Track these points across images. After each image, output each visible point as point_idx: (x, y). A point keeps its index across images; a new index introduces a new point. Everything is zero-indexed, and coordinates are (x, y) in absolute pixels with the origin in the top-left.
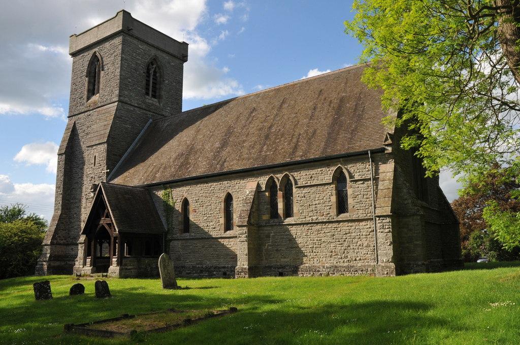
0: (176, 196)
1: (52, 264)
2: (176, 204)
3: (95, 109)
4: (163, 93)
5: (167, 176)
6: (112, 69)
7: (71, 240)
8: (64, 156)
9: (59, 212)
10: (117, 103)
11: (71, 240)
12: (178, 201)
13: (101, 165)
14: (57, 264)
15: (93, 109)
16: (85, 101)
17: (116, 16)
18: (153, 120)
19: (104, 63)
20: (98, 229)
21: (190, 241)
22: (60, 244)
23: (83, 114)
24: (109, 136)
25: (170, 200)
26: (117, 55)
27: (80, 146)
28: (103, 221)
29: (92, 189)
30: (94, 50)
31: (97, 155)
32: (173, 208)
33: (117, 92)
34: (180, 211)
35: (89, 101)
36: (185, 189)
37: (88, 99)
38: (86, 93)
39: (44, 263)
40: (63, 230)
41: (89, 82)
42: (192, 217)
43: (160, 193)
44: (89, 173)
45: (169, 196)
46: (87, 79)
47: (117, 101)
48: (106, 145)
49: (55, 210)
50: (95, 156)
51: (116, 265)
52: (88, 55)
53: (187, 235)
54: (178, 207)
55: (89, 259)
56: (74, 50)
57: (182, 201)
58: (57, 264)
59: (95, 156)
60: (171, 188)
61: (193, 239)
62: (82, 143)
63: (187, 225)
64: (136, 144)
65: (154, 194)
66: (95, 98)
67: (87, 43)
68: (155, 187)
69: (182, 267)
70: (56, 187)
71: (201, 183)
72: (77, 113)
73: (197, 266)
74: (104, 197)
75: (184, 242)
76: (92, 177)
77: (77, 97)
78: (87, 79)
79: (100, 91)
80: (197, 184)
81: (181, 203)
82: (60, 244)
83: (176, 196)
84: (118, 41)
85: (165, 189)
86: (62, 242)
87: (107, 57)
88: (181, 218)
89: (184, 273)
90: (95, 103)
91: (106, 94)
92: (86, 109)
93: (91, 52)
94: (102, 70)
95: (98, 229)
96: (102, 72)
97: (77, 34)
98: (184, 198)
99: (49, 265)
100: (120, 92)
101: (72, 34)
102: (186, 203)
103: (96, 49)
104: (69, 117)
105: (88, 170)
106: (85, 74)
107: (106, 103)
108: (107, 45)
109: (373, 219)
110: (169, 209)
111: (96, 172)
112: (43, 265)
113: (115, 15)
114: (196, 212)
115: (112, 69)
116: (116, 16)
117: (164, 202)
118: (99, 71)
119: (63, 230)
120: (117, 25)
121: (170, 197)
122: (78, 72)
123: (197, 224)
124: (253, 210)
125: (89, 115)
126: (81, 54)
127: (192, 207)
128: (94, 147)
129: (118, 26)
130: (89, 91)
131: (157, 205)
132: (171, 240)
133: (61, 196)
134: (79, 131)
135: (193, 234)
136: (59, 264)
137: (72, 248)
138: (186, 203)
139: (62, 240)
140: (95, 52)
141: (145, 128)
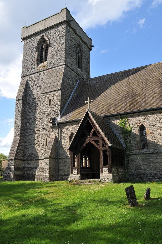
0: (133, 124)
1: (16, 173)
2: (133, 129)
3: (44, 70)
4: (83, 66)
5: (121, 109)
6: (57, 45)
7: (27, 157)
8: (21, 101)
9: (19, 138)
10: (64, 65)
11: (27, 157)
12: (135, 127)
13: (56, 105)
14: (19, 173)
15: (43, 71)
16: (35, 66)
17: (60, 13)
18: (80, 81)
19: (51, 42)
20: (84, 145)
21: (149, 155)
22: (19, 160)
23: (34, 75)
24: (61, 86)
25: (127, 126)
26: (62, 36)
27: (32, 94)
28: (90, 139)
29: (50, 120)
30: (42, 35)
31: (52, 98)
32: (131, 132)
33: (64, 59)
34: (138, 133)
35: (39, 66)
36: (141, 118)
37: (38, 65)
38: (36, 61)
39: (10, 172)
40: (21, 150)
41: (38, 55)
42: (149, 137)
43: (117, 122)
44: (44, 111)
45: (125, 123)
46: (36, 53)
47: (64, 64)
48: (60, 92)
49: (15, 137)
50: (50, 100)
51: (107, 173)
52: (37, 39)
53: (145, 151)
54: (136, 130)
55: (107, 167)
56: (26, 35)
57: (139, 126)
58: (19, 173)
59: (50, 100)
60: (127, 117)
61: (153, 153)
62: (34, 93)
63: (144, 143)
64: (74, 94)
65: (111, 122)
66: (45, 64)
67: (36, 31)
68: (112, 117)
69: (144, 174)
70: (15, 122)
71: (157, 113)
72: (29, 74)
73: (159, 173)
74: (92, 121)
75: (143, 156)
76: (48, 114)
77: (28, 64)
78: (36, 53)
79: (49, 59)
80: (153, 114)
81: (138, 128)
82: (19, 160)
83: (133, 124)
84: (62, 28)
85: (122, 118)
86: (20, 158)
87: (53, 38)
88: (138, 139)
89: (145, 179)
90: (44, 67)
91: (53, 61)
92: (37, 71)
93: (39, 37)
94: (50, 46)
95: (84, 145)
96: (49, 48)
97: (27, 26)
98: (140, 124)
99: (15, 173)
100: (66, 59)
101: (24, 26)
102: (142, 128)
103: (44, 34)
104: (22, 77)
105: (44, 109)
106: (35, 49)
107: (54, 66)
108: (53, 31)
109: (57, 159)
110: (127, 133)
111: (52, 110)
112: (9, 173)
113: (59, 12)
114: (153, 134)
115: (57, 45)
116: (60, 13)
117: (121, 128)
118: (47, 47)
119: (21, 150)
120: (62, 17)
121: (127, 124)
122: (29, 49)
123: (155, 142)
124: (53, 150)
125: (40, 75)
126: (30, 38)
127: (148, 131)
128: (49, 94)
129: (63, 17)
130: (38, 60)
131: (114, 130)
132: (130, 155)
133: (20, 127)
134: (31, 86)
135: (152, 150)
136: (19, 173)
137: (28, 163)
138: (142, 128)
139: (21, 157)
140: (43, 36)
141: (77, 85)
